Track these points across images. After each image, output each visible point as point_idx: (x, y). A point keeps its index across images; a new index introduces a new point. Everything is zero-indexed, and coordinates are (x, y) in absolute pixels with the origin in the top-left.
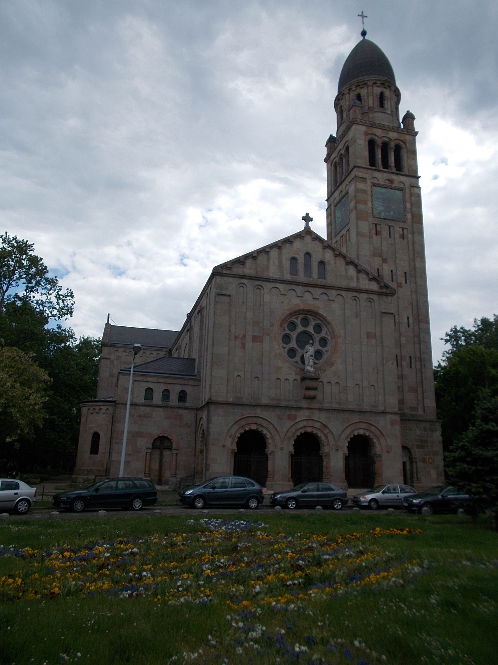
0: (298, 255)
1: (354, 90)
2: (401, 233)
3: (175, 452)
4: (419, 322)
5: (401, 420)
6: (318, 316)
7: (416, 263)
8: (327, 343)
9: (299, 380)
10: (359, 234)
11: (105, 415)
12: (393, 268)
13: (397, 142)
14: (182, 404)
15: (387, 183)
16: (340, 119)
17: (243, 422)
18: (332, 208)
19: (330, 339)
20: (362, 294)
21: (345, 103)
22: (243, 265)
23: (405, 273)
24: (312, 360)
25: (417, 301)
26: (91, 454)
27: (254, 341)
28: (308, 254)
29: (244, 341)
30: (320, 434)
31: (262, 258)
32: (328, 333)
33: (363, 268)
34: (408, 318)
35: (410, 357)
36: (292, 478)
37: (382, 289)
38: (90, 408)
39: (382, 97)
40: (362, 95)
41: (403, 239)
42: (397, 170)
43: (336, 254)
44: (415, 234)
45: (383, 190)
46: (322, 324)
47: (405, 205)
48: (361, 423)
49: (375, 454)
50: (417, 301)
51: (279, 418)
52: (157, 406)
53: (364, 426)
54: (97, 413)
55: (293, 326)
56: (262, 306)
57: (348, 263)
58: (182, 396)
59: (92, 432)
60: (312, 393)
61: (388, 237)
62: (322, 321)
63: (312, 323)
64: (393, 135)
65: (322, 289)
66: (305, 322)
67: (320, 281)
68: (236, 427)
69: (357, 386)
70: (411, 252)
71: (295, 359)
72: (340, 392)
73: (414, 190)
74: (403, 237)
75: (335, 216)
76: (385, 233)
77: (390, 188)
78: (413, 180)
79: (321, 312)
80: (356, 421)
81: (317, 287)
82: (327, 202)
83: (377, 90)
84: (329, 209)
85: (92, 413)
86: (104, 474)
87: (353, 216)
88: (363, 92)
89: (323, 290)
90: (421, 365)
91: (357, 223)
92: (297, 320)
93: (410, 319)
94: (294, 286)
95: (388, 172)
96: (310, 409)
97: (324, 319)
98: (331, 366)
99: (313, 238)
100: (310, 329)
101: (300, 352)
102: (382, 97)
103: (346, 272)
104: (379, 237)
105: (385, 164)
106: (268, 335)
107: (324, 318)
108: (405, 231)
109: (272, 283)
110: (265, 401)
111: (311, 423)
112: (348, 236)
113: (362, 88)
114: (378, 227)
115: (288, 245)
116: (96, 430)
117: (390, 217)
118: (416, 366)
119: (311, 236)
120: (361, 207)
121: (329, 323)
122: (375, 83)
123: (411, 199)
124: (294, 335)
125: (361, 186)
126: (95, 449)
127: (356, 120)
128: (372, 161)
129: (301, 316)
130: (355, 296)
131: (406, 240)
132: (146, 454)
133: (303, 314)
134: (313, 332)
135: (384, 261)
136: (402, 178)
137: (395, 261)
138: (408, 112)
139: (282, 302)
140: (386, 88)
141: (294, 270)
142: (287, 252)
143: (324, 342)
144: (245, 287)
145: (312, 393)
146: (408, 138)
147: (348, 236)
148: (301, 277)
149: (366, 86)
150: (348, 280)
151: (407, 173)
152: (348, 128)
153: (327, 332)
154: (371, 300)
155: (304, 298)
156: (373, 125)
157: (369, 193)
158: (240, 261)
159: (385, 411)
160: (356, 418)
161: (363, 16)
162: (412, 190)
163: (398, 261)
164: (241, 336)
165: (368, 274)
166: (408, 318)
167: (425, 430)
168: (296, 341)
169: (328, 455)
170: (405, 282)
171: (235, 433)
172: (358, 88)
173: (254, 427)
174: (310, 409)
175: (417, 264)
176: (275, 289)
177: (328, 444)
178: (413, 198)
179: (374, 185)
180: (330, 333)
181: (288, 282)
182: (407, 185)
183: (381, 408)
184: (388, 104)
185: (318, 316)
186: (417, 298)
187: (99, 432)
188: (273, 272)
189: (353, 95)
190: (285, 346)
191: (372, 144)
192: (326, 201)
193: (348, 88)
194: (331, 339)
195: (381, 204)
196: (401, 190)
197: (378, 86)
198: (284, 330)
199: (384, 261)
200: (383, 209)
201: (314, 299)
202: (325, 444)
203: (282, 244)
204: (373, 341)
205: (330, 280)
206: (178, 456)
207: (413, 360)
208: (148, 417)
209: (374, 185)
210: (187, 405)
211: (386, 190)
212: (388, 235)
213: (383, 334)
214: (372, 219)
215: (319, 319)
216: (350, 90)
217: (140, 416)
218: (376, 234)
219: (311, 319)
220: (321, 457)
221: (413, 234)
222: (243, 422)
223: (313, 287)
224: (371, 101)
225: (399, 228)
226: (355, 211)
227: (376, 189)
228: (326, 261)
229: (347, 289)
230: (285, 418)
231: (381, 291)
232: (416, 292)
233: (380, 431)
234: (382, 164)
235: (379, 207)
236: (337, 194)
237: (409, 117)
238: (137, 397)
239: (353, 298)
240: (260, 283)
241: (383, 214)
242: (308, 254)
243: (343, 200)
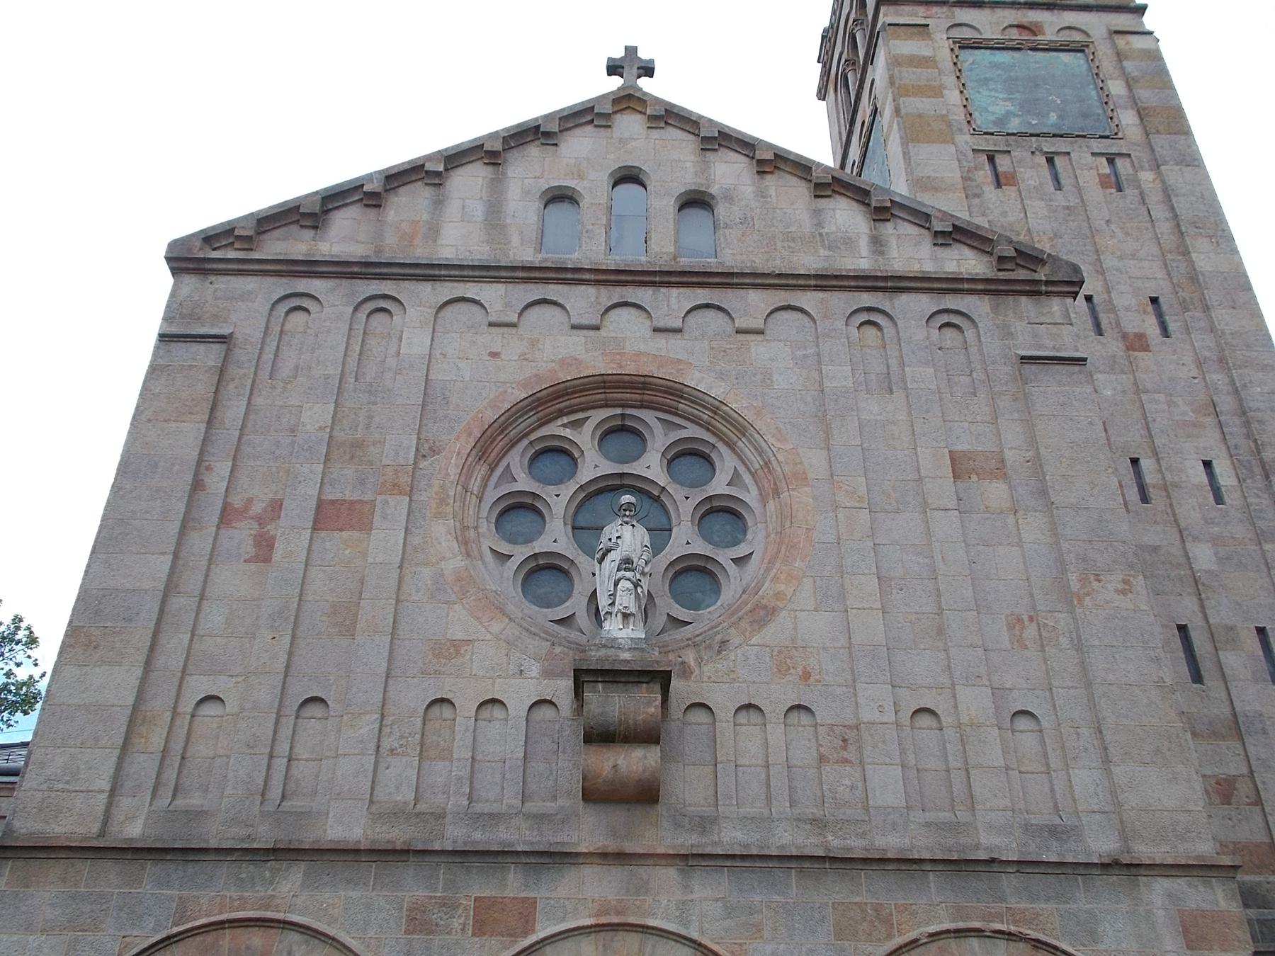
0: (581, 177)
20: (904, 298)
22: (316, 228)
32: (747, 478)
33: (897, 199)
34: (1207, 464)
41: (1120, 189)
44: (1162, 167)
46: (712, 439)
48: (974, 942)
50: (1236, 391)
61: (1050, 187)
62: (707, 427)
63: (659, 439)
65: (699, 291)
69: (925, 721)
70: (1165, 227)
72: (822, 759)
77: (1031, 49)
80: (933, 928)
81: (669, 284)
93: (1223, 469)
96: (620, 858)
98: (761, 623)
103: (819, 225)
104: (1010, 191)
107: (716, 409)
114: (999, 160)
121: (742, 429)
123: (1123, 69)
131: (1130, 192)
139: (494, 355)
150: (830, 248)
155: (603, 332)
159: (1126, 860)
164: (257, 508)
165: (928, 217)
166: (1207, 464)
170: (1158, 331)
175: (1204, 259)
178: (1125, 63)
179: (965, 45)
181: (520, 274)
183: (1101, 845)
186: (1232, 382)
194: (763, 499)
198: (508, 476)
201: (657, 330)
204: (996, 493)
209: (965, 45)
211: (1016, 54)
213: (1043, 451)
214: (968, 137)
215: (695, 421)
218: (999, 185)
221: (1157, 166)
223: (653, 284)
225: (1090, 159)
227: (968, 57)
228: (714, 190)
229: (826, 282)
230: (456, 923)
231: (1002, 275)
232: (1222, 360)
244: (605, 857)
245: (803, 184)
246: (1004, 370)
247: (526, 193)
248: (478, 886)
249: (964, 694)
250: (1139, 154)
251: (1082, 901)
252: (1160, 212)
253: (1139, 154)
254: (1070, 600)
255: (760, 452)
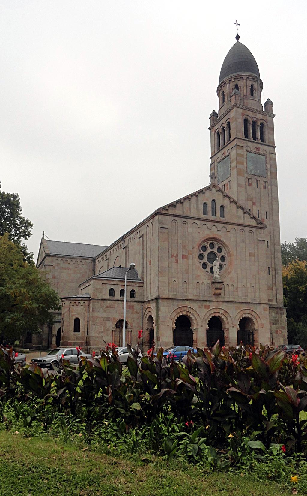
1: (234, 81)
2: (264, 185)
3: (130, 330)
4: (274, 245)
5: (269, 308)
6: (220, 242)
7: (273, 205)
8: (225, 260)
9: (210, 283)
10: (239, 185)
11: (83, 306)
12: (259, 209)
13: (262, 121)
14: (112, 298)
15: (256, 150)
16: (222, 102)
17: (179, 310)
18: (216, 163)
19: (227, 257)
21: (227, 89)
23: (266, 212)
24: (218, 271)
25: (273, 231)
26: (74, 332)
27: (183, 258)
28: (214, 201)
29: (177, 258)
30: (223, 317)
31: (186, 203)
32: (226, 253)
35: (269, 267)
36: (207, 344)
37: (258, 224)
38: (72, 302)
39: (252, 88)
40: (239, 86)
42: (261, 142)
43: (231, 201)
45: (253, 155)
47: (266, 166)
49: (254, 329)
50: (273, 231)
51: (200, 307)
52: (118, 300)
53: (248, 312)
54: (77, 305)
55: (204, 248)
56: (187, 235)
57: (238, 207)
58: (133, 294)
59: (74, 318)
60: (218, 291)
62: (222, 245)
64: (260, 116)
65: (223, 224)
66: (212, 246)
67: (222, 219)
68: (175, 313)
70: (270, 198)
71: (206, 270)
72: (234, 291)
73: (272, 156)
74: (265, 187)
75: (218, 170)
76: (254, 185)
78: (272, 148)
79: (222, 239)
82: (210, 159)
83: (249, 83)
84: (213, 165)
85: (73, 305)
86: (85, 345)
87: (234, 172)
88: (240, 84)
89: (223, 225)
90: (275, 272)
91: (237, 177)
92: (207, 244)
94: (206, 222)
95: (257, 143)
96: (217, 301)
97: (223, 244)
99: (217, 190)
100: (215, 250)
101: (209, 265)
102: (252, 88)
104: (250, 187)
105: (255, 138)
106: (191, 254)
108: (267, 183)
109: (193, 220)
110: (191, 297)
111: (218, 310)
112: (229, 185)
113: (240, 80)
114: (250, 180)
115: (201, 194)
116: (77, 316)
117: (257, 174)
118: (272, 273)
119: (216, 188)
120: (240, 166)
121: (227, 247)
122: (248, 78)
123: (270, 162)
124: (206, 254)
125: (240, 151)
126: (77, 329)
127: (237, 105)
128: (246, 136)
129: (210, 242)
130: (242, 229)
131: (267, 190)
132: (112, 332)
133: (210, 241)
134: (217, 253)
135: (254, 204)
136: (265, 147)
137: (261, 204)
138: (268, 99)
139: (199, 233)
140: (255, 82)
141: (205, 213)
142: (202, 199)
143: (223, 258)
144: (186, 224)
145: (218, 291)
146: (269, 119)
147: (229, 185)
148: (210, 216)
149: (242, 79)
151: (268, 144)
152: (230, 110)
153: (225, 252)
154: (251, 232)
156: (247, 109)
157: (245, 156)
158: (172, 205)
160: (244, 307)
161: (237, 24)
162: (271, 156)
163: (262, 205)
164: (175, 255)
167: (277, 313)
168: (207, 258)
169: (228, 330)
171: (174, 317)
172: (236, 80)
173: (185, 313)
174: (217, 301)
176: (205, 225)
177: (228, 323)
178: (271, 161)
179: (248, 151)
180: (227, 253)
182: (268, 152)
183: (258, 301)
184: (256, 93)
185: (220, 242)
187: (79, 318)
188: (193, 213)
189: (232, 85)
190: (200, 261)
191: (246, 121)
192: (210, 158)
193: (229, 80)
194: (228, 256)
195: (252, 165)
196: (264, 155)
197: (250, 80)
198: (200, 251)
199: (254, 204)
200: (253, 168)
201: (218, 230)
202: (226, 323)
203: (199, 194)
204: (253, 258)
205: (226, 219)
206: (132, 332)
207: (270, 269)
208: (113, 308)
209: (248, 151)
210: (136, 299)
212: (256, 186)
215: (221, 244)
216: (230, 81)
217: (107, 307)
219: (216, 244)
220: (223, 331)
221: (271, 186)
222: (179, 310)
224: (245, 91)
226: (236, 169)
227: (248, 154)
228: (225, 205)
229: (238, 225)
233: (258, 315)
234: (252, 137)
235: (251, 167)
236: (219, 154)
237: (269, 103)
238: (105, 294)
239: (241, 230)
240: (185, 220)
241: (253, 171)
242: (214, 201)
243: (225, 159)
244: (216, 301)
245: (235, 205)
246: (256, 241)
247: (201, 203)
248: (205, 304)
249: (248, 284)
250: (269, 182)
251: (256, 306)
252: (270, 195)
253: (269, 182)
254: (259, 273)
255: (229, 250)
